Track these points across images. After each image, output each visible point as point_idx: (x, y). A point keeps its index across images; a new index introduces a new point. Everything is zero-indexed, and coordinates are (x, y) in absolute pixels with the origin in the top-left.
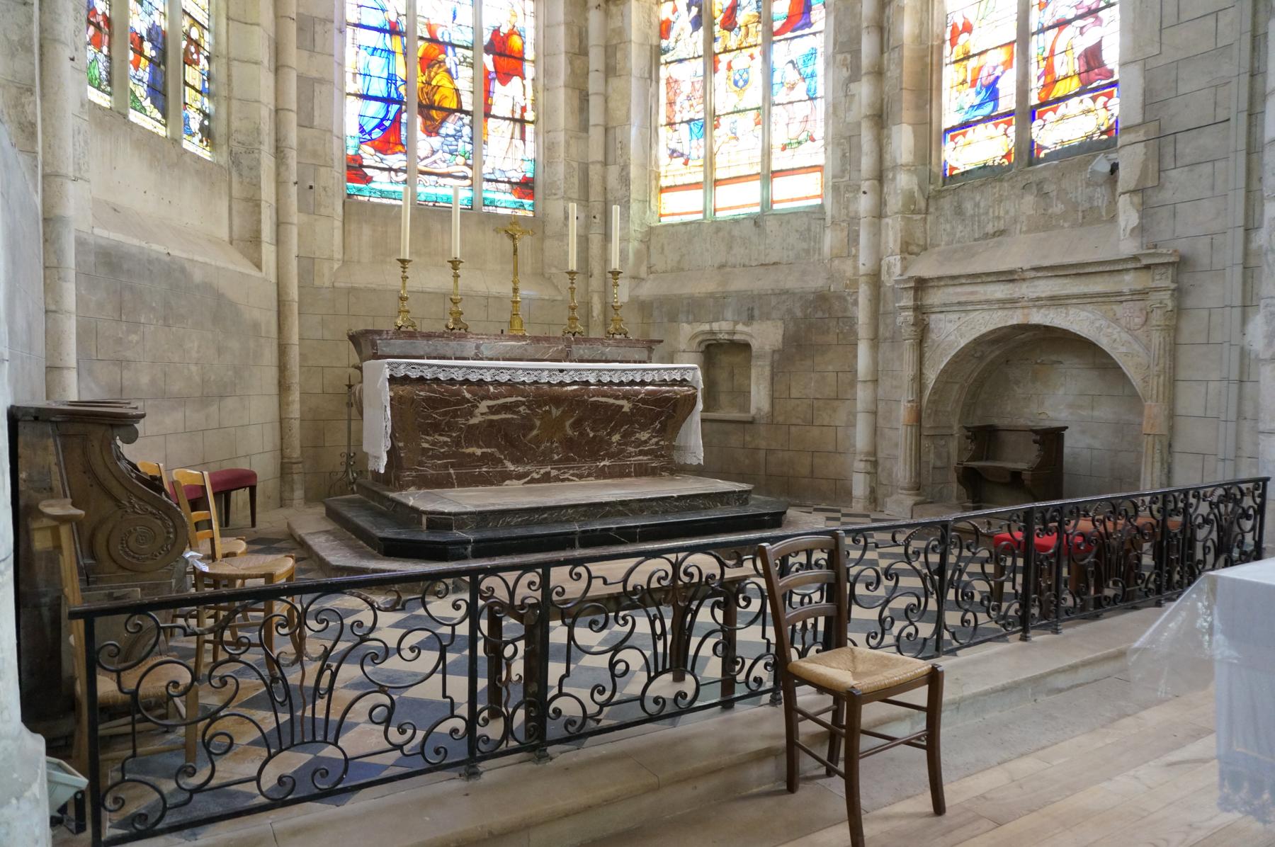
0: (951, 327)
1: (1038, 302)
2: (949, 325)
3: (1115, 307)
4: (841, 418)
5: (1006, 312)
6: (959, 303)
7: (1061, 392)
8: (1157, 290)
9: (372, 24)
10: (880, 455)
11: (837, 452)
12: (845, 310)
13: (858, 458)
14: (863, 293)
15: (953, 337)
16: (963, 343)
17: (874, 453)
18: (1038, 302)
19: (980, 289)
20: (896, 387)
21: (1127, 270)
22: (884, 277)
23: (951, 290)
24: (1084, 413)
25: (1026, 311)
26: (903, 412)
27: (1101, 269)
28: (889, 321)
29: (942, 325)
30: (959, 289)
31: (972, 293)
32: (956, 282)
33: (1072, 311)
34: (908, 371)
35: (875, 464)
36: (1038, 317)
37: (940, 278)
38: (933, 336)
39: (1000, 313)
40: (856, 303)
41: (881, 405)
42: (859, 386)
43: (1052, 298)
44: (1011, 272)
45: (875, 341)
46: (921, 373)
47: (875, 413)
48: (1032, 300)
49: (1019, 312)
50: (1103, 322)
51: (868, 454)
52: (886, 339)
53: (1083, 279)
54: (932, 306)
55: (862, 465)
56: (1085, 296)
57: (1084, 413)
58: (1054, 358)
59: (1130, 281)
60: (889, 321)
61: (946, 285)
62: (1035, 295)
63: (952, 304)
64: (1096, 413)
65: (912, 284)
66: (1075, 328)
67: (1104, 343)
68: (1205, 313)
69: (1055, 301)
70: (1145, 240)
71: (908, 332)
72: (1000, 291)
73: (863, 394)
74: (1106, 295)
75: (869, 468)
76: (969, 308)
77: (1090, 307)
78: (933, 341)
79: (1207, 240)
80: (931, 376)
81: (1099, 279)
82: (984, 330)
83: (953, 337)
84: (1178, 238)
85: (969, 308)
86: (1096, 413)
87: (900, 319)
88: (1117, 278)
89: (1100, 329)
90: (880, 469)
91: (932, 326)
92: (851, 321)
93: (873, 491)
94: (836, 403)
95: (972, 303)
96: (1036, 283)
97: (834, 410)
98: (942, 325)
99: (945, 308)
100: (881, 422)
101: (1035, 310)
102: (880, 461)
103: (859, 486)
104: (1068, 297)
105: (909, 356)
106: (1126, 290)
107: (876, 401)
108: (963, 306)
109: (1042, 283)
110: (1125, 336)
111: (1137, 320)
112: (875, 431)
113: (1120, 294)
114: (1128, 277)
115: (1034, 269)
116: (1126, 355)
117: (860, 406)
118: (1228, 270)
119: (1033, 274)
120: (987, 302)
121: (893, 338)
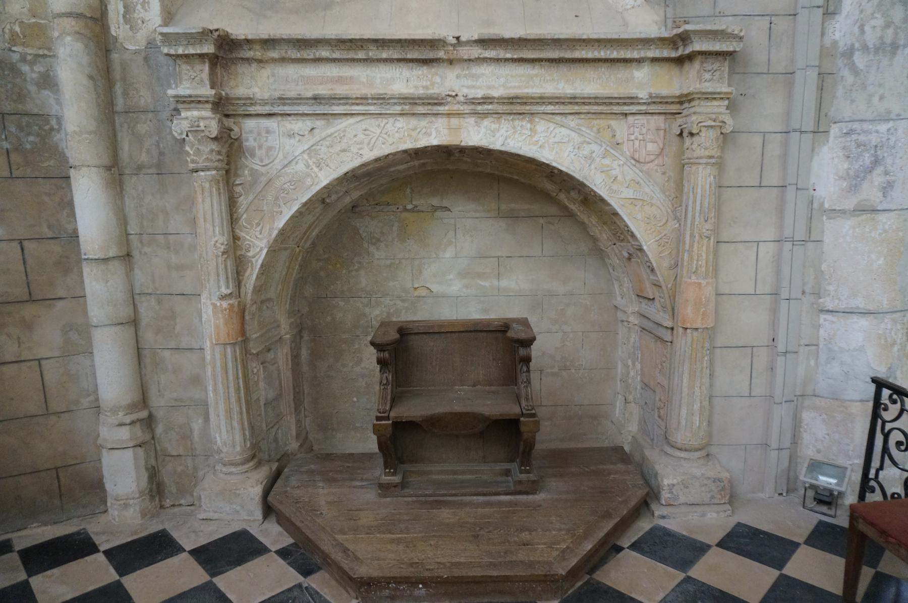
0: (295, 147)
1: (483, 107)
2: (288, 143)
3: (613, 123)
4: (48, 337)
5: (413, 122)
6: (316, 99)
7: (449, 253)
8: (709, 97)
9: (46, 378)
10: (157, 402)
11: (48, 413)
12: (21, 97)
13: (114, 420)
14: (70, 64)
15: (300, 167)
16: (325, 178)
17: (143, 401)
18: (483, 107)
19: (359, 73)
20: (180, 267)
21: (639, 61)
22: (117, 28)
23: (291, 71)
24: (487, 284)
25: (454, 121)
26: (210, 317)
27: (603, 54)
28: (142, 128)
29: (272, 141)
30: (310, 71)
31: (340, 80)
32: (309, 54)
33: (542, 126)
34: (213, 237)
35: (149, 422)
36: (477, 134)
37: (269, 43)
38: (253, 164)
39: (401, 123)
40: (48, 81)
41: (147, 310)
42: (90, 274)
43: (511, 100)
44: (433, 44)
45: (115, 173)
46: (235, 238)
47: (135, 322)
48: (473, 102)
49: (441, 122)
50: (594, 147)
51: (133, 407)
52: (140, 168)
53: (564, 69)
54: (251, 101)
55: (124, 434)
56: (573, 100)
57: (487, 284)
58: (435, 201)
59: (643, 81)
60: (142, 128)
61: (283, 60)
62: (480, 93)
63: (299, 100)
64: (504, 283)
65: (208, 48)
66: (546, 156)
67: (598, 184)
68: (758, 140)
69: (516, 106)
70: (670, 12)
71: (202, 154)
72: (402, 81)
73: (100, 290)
74: (608, 101)
75: (139, 433)
76: (338, 109)
77: (572, 121)
78: (254, 173)
79: (764, 23)
80: (258, 244)
81: (590, 72)
82: (369, 155)
83: (300, 167)
84: (722, 15)
85: (338, 109)
86: (504, 283)
87: (180, 127)
88: (622, 73)
89: (590, 158)
90: (159, 429)
91: (250, 142)
92: (44, 126)
93: (153, 475)
94: (29, 311)
95: (345, 99)
96: (476, 70)
97: (28, 326)
98: (272, 141)
99: (281, 108)
100: (148, 337)
101: (471, 120)
102: (160, 414)
103: (122, 474)
104: (542, 100)
105: (208, 205)
106: (643, 95)
107: (133, 298)
108: (323, 107)
109: (486, 70)
110: (631, 173)
111: (651, 147)
112: (140, 357)
113: (631, 100)
114: (641, 74)
115: (484, 42)
116: (633, 201)
117: (97, 312)
118: (798, 74)
119: (476, 52)
120: (381, 99)
121: (159, 165)
